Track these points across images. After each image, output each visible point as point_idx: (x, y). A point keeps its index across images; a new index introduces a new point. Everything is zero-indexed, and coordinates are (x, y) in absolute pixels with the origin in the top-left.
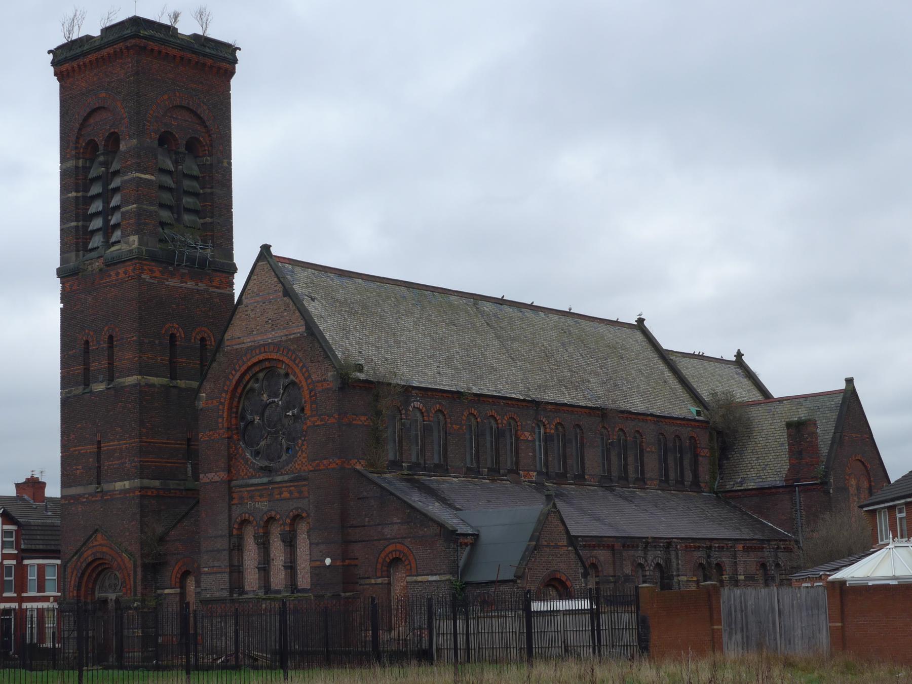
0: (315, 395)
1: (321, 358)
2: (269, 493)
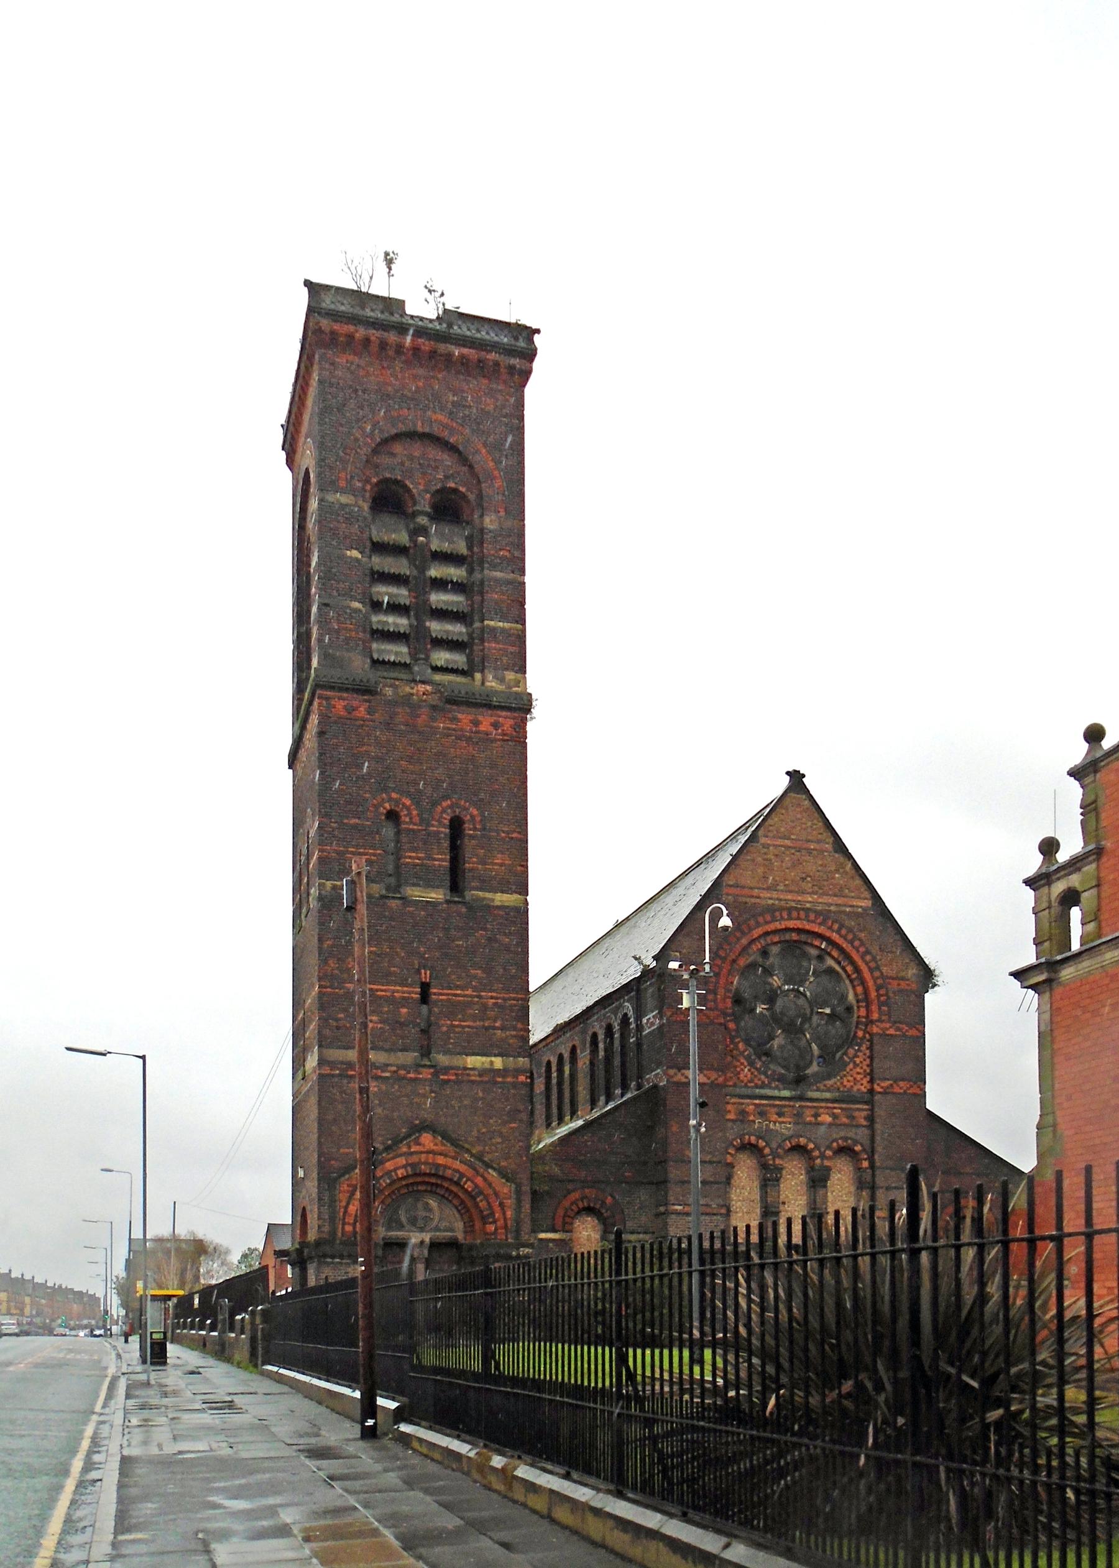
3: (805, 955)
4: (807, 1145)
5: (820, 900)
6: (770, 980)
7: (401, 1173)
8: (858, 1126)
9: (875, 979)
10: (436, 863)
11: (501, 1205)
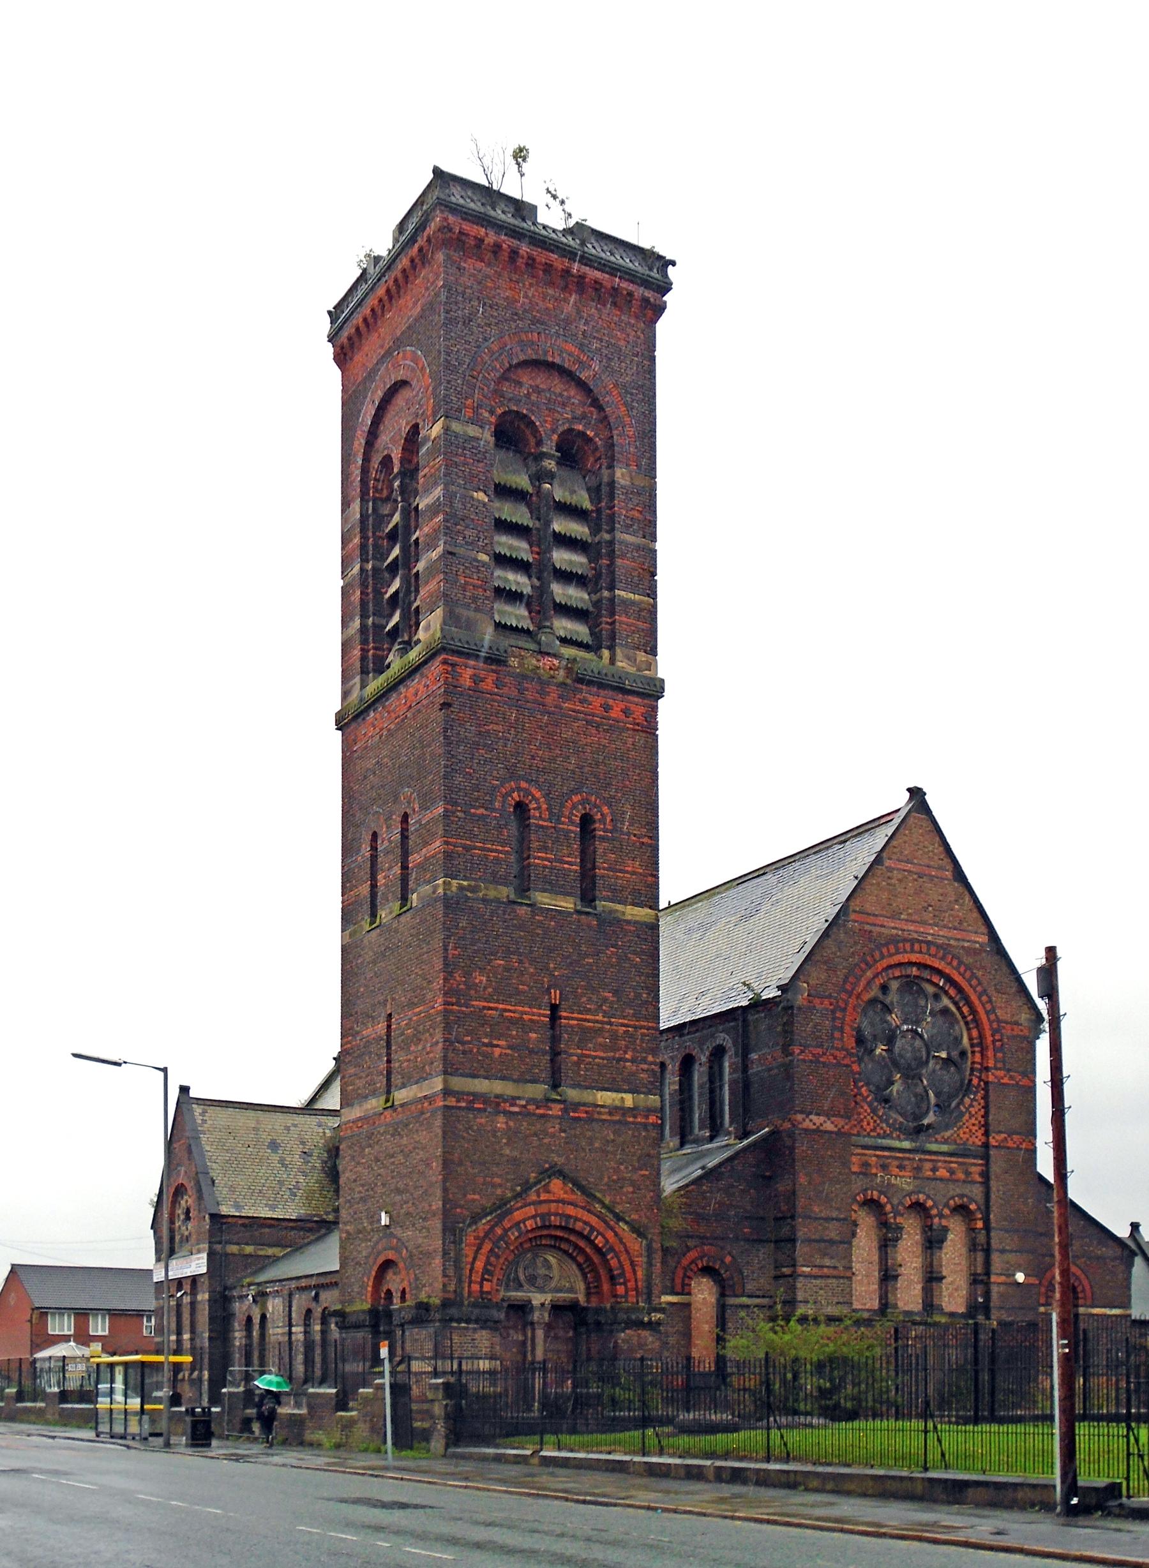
2: (915, 1166)
3: (921, 991)
4: (925, 1201)
5: (941, 933)
6: (889, 1018)
7: (530, 1224)
8: (973, 1182)
9: (991, 1022)
10: (566, 866)
11: (632, 1263)
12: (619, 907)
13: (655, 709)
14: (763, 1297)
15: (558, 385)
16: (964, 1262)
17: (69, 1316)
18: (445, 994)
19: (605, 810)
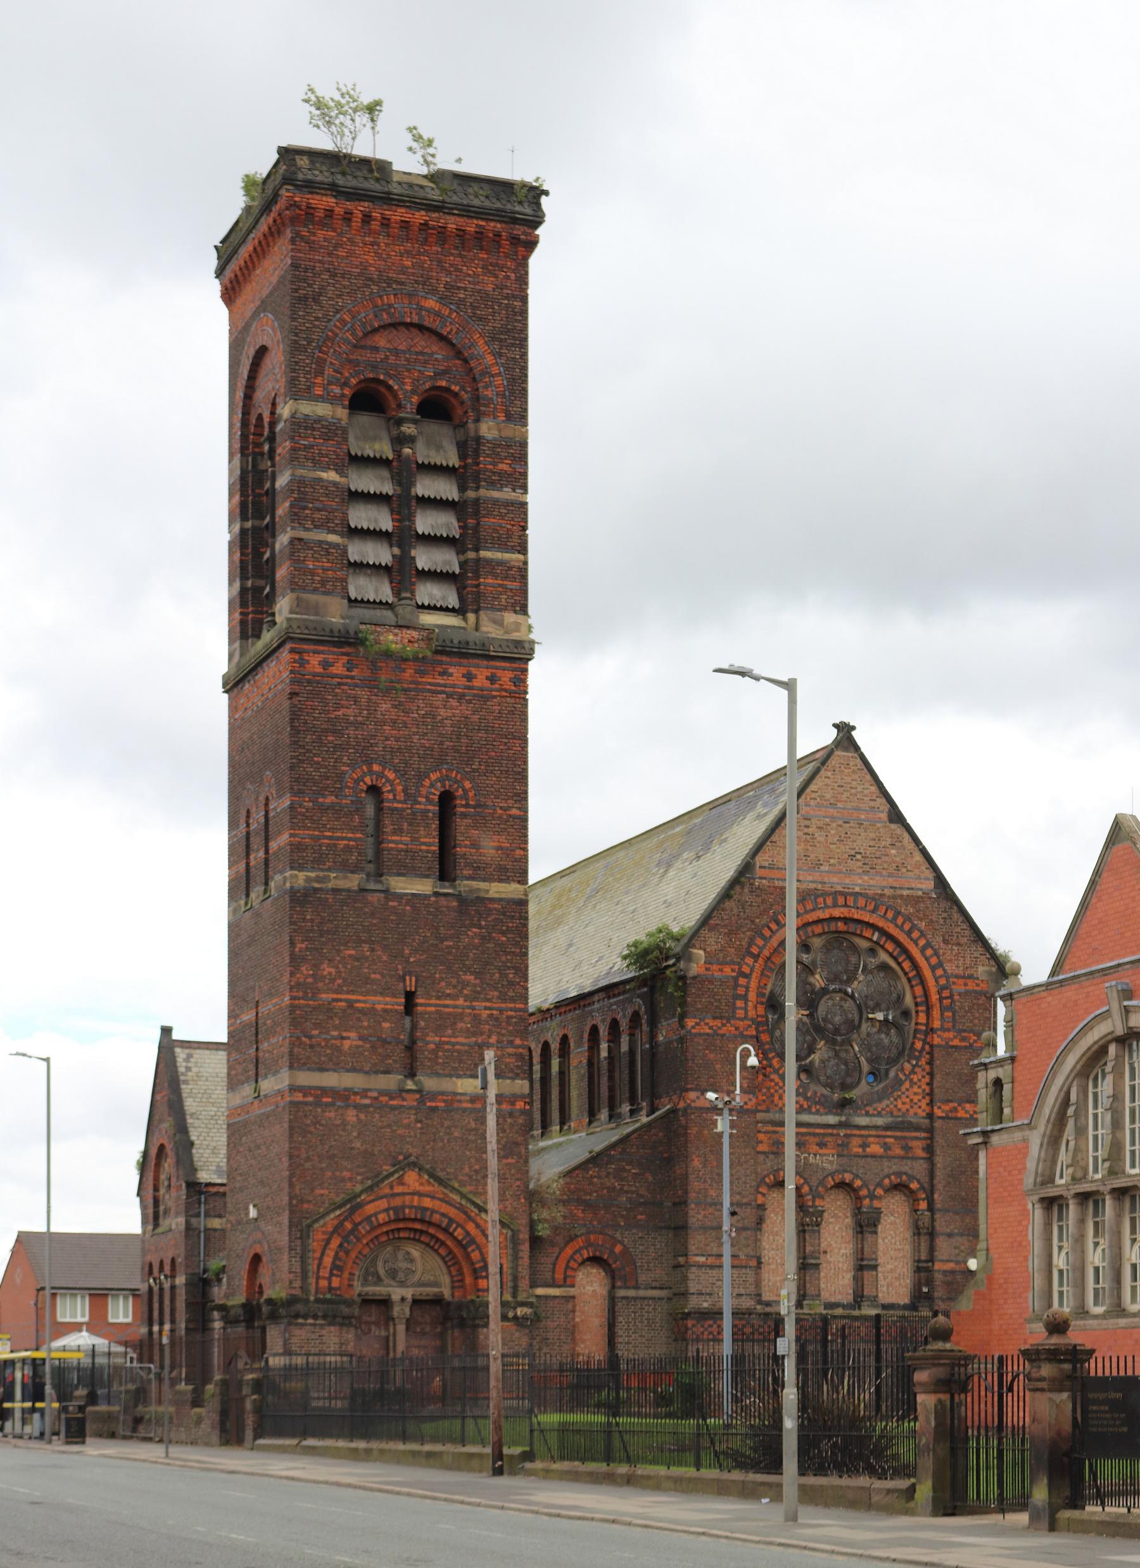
0: (951, 997)
1: (964, 940)
3: (854, 948)
7: (382, 1217)
12: (483, 885)
13: (525, 671)
14: (661, 1288)
15: (421, 343)
16: (908, 1247)
17: (83, 1297)
18: (291, 988)
19: (467, 784)
